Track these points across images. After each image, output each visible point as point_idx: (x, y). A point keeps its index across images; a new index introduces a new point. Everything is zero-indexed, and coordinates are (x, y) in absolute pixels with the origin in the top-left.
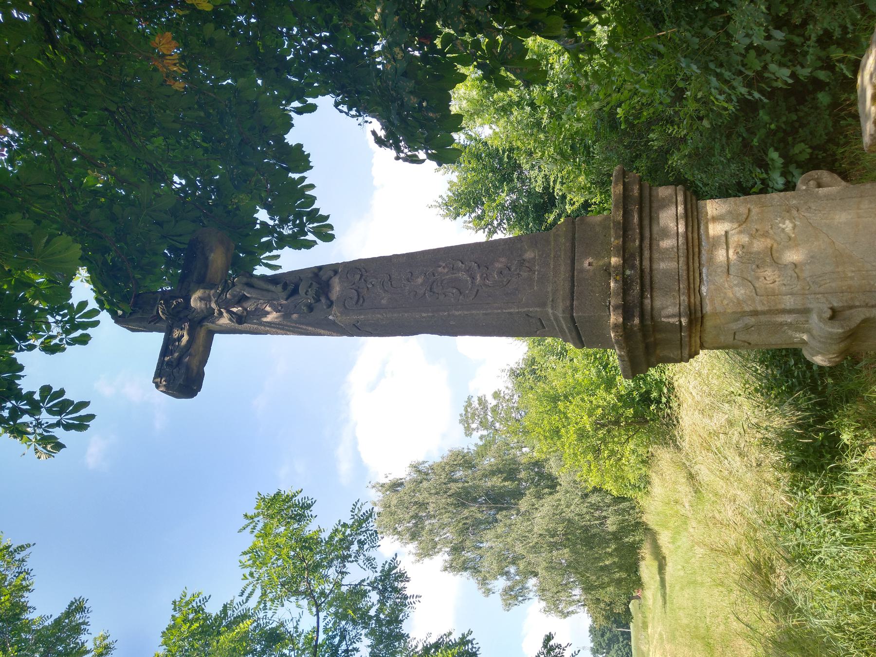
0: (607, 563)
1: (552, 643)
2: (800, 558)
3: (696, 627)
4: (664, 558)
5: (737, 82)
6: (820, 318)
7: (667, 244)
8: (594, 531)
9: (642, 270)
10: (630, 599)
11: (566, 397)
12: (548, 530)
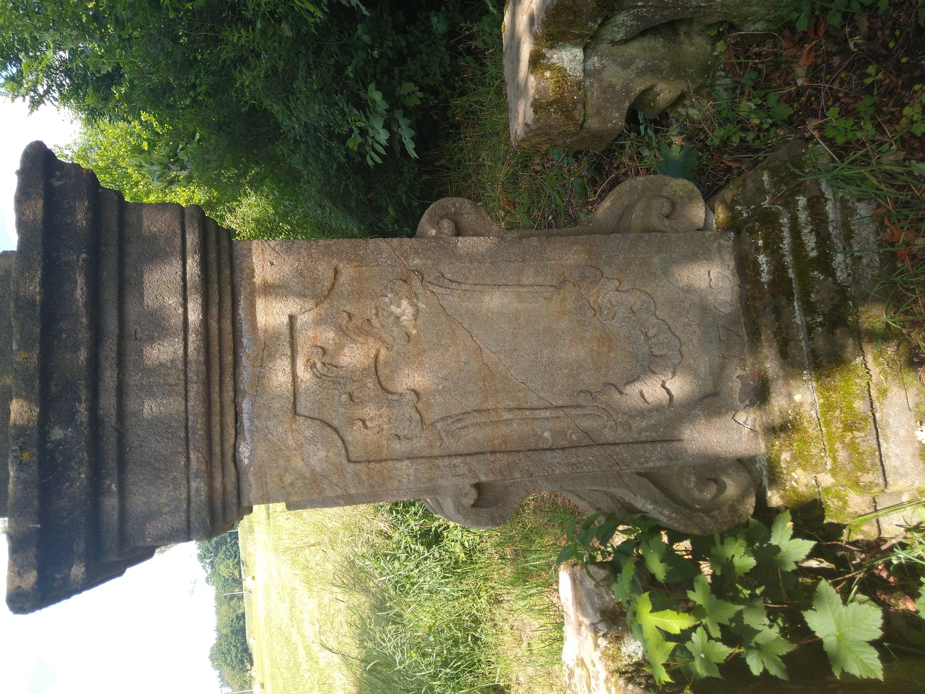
7: (162, 352)
9: (95, 421)
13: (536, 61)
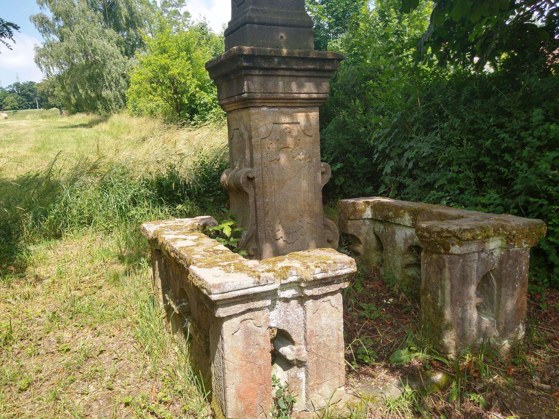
0: (80, 91)
1: (12, 29)
2: (105, 187)
3: (49, 144)
4: (91, 127)
5: (385, 144)
6: (248, 172)
7: (294, 87)
8: (101, 83)
9: (277, 69)
10: (59, 108)
11: (189, 59)
12: (95, 48)
13: (368, 203)
